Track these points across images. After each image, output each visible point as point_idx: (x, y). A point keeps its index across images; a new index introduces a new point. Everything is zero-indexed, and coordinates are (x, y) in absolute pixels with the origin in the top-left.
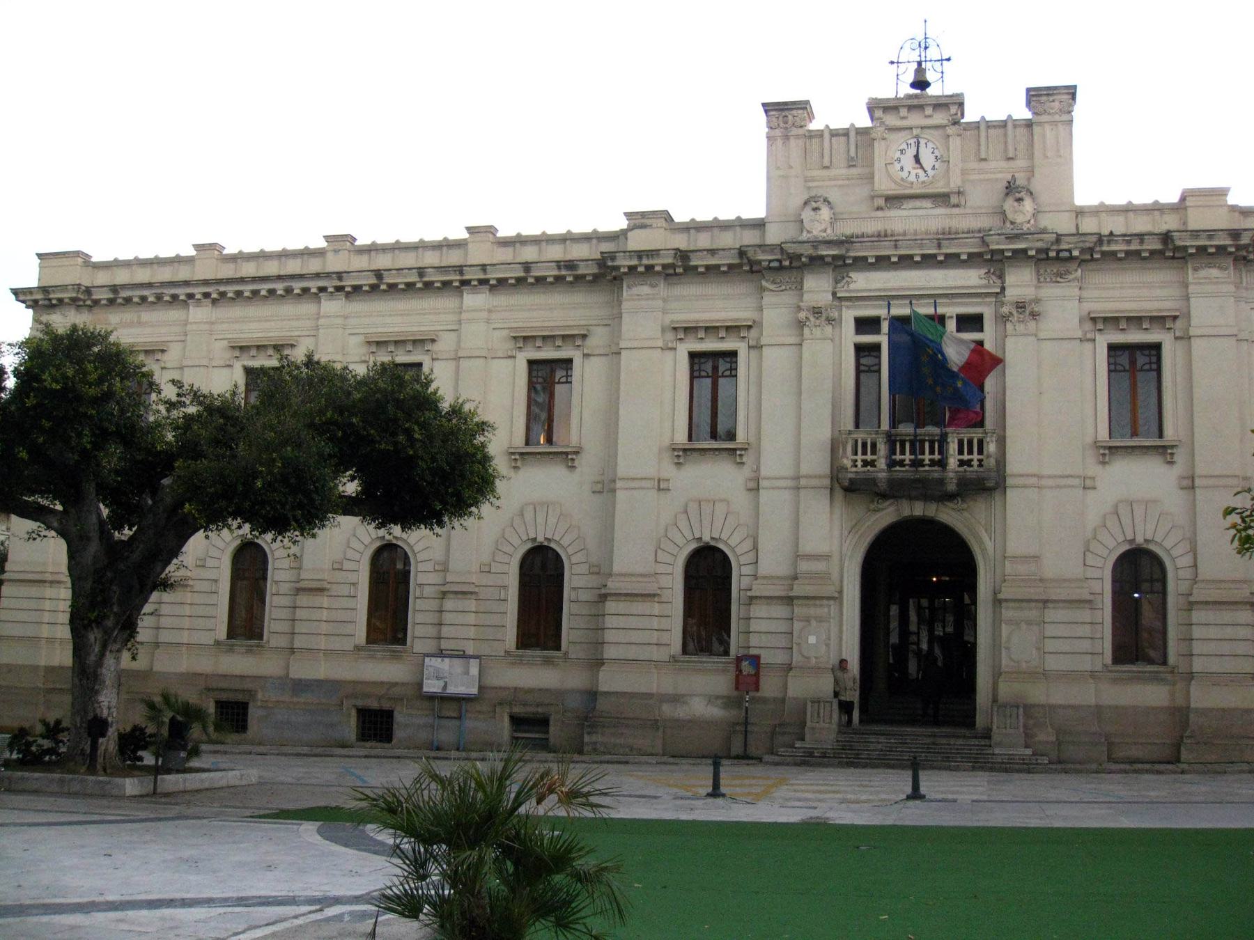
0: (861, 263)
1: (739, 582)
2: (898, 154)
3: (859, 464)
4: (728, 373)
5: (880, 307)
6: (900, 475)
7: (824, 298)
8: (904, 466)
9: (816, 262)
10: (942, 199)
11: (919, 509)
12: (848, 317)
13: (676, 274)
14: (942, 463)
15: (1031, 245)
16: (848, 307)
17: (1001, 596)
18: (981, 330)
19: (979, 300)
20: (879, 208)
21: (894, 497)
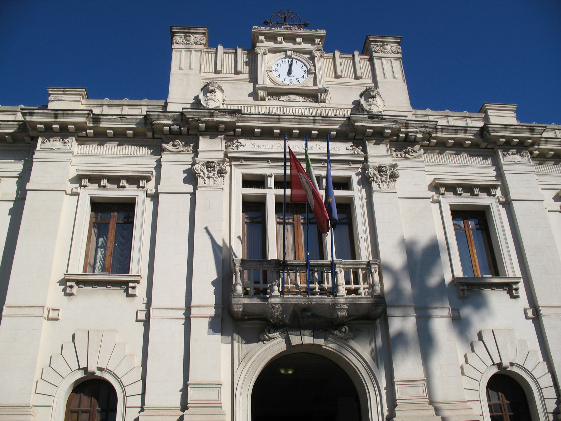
0: (249, 133)
2: (275, 67)
5: (278, 167)
7: (387, 161)
8: (314, 294)
9: (213, 131)
10: (313, 96)
12: (238, 173)
13: (87, 136)
15: (388, 128)
16: (236, 166)
18: (244, 197)
19: (346, 166)
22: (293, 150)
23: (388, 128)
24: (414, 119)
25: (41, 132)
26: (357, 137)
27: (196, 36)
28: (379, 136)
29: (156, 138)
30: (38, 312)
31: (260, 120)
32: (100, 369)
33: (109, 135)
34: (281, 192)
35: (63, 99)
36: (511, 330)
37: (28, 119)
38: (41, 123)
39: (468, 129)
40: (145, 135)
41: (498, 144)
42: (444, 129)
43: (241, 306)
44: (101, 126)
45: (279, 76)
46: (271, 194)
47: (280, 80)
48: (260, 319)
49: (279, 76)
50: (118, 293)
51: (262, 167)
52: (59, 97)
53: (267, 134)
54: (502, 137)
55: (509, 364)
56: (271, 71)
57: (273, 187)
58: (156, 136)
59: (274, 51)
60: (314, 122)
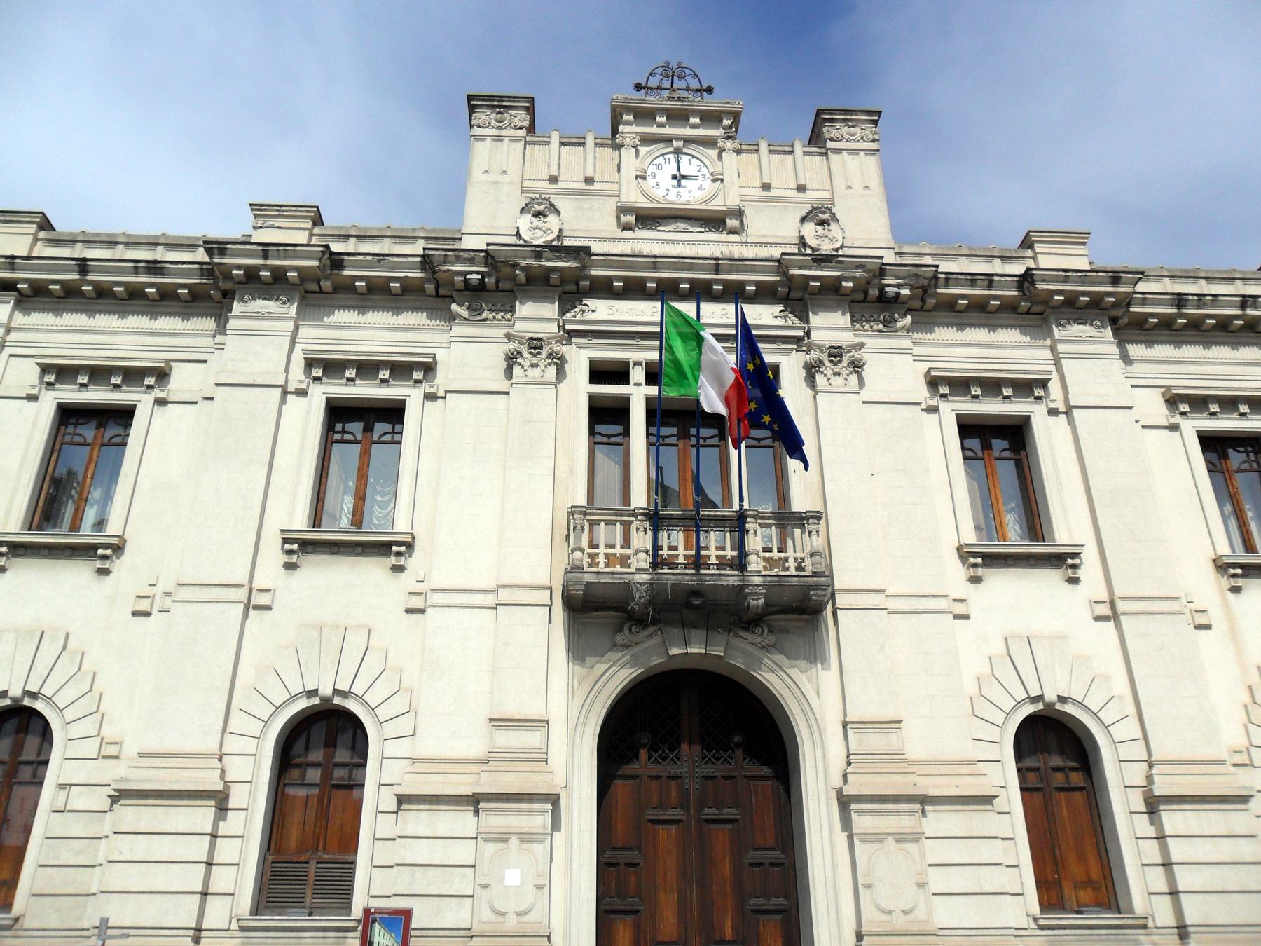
0: (605, 289)
1: (382, 776)
3: (602, 560)
4: (388, 438)
6: (671, 580)
7: (845, 337)
8: (676, 566)
10: (713, 221)
11: (694, 648)
12: (579, 359)
13: (321, 291)
14: (740, 564)
16: (580, 346)
17: (848, 790)
18: (593, 399)
20: (626, 227)
21: (655, 622)
22: (750, 321)
23: (847, 279)
24: (898, 261)
25: (239, 283)
26: (792, 295)
27: (513, 113)
28: (830, 294)
29: (444, 296)
30: (941, 604)
31: (620, 266)
32: (1062, 699)
33: (360, 290)
34: (653, 390)
35: (277, 224)
36: (1062, 637)
37: (216, 260)
38: (239, 267)
39: (996, 278)
40: (423, 290)
41: (1052, 304)
42: (950, 278)
43: (582, 587)
44: (345, 273)
45: (657, 185)
46: (638, 394)
47: (659, 194)
48: (616, 609)
49: (657, 185)
50: (1051, 578)
51: (624, 348)
52: (271, 222)
53: (634, 290)
54: (1059, 292)
55: (1055, 698)
56: (644, 178)
57: (644, 382)
58: (441, 292)
59: (647, 140)
60: (265, 255)
